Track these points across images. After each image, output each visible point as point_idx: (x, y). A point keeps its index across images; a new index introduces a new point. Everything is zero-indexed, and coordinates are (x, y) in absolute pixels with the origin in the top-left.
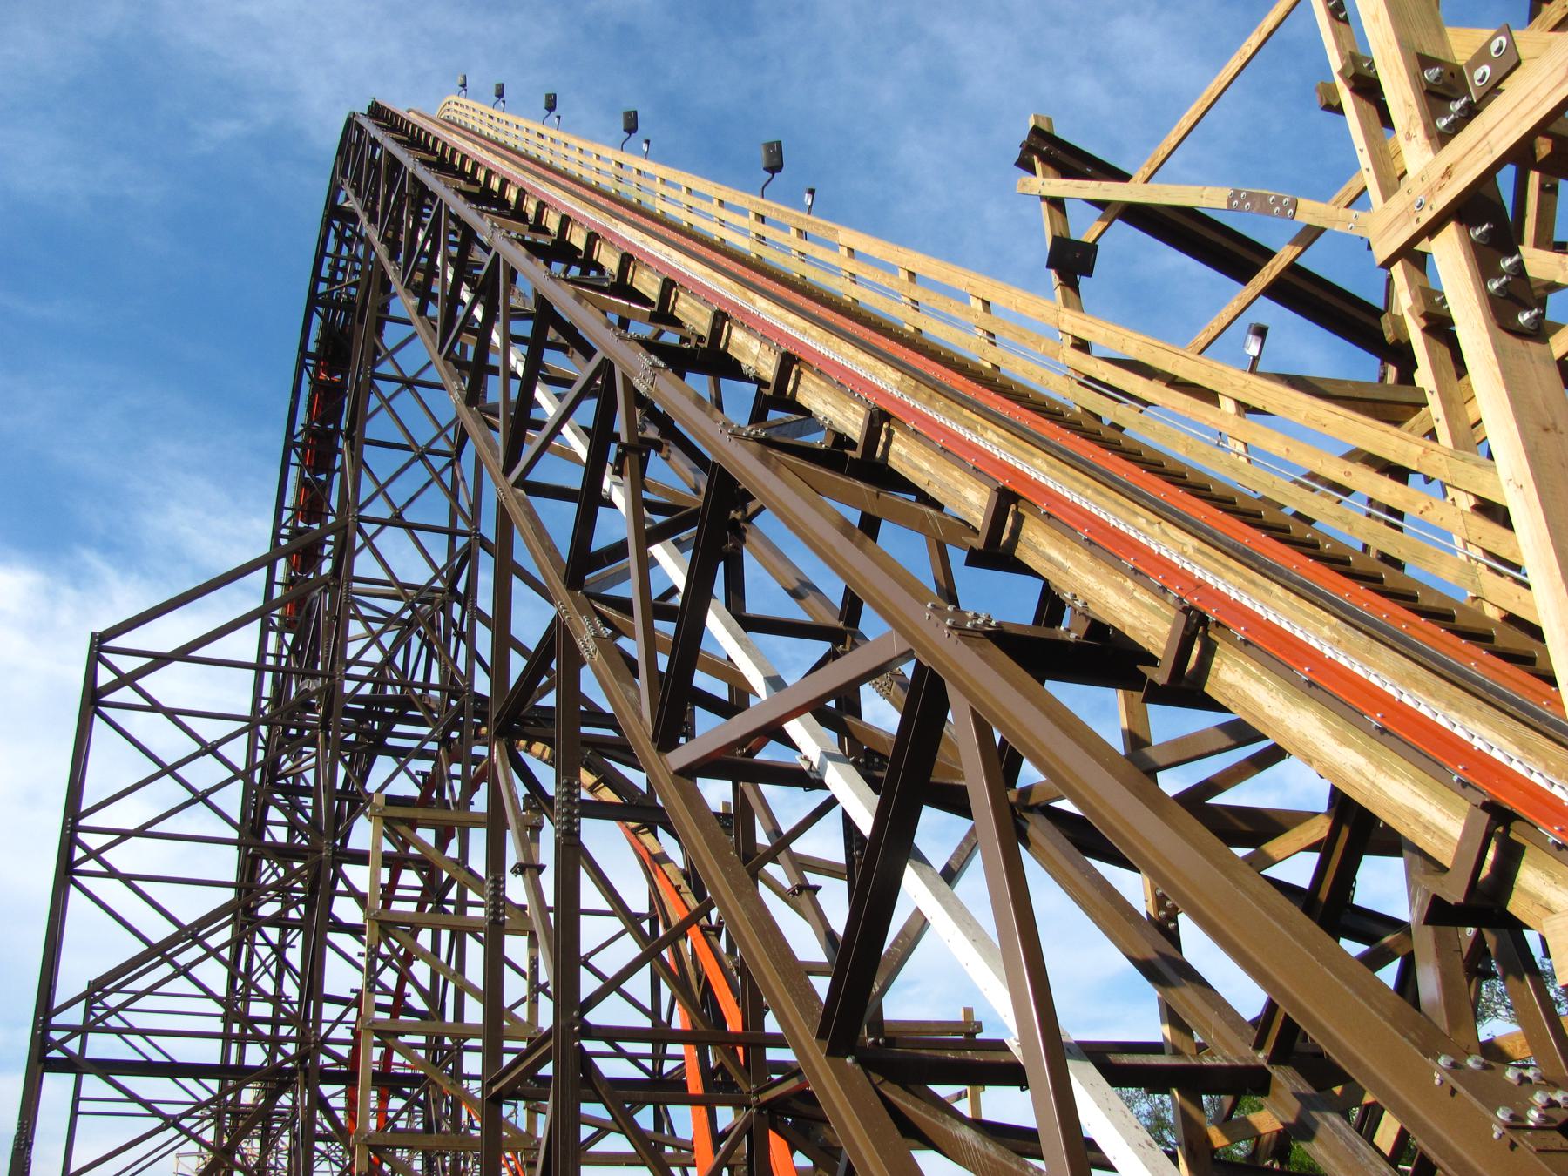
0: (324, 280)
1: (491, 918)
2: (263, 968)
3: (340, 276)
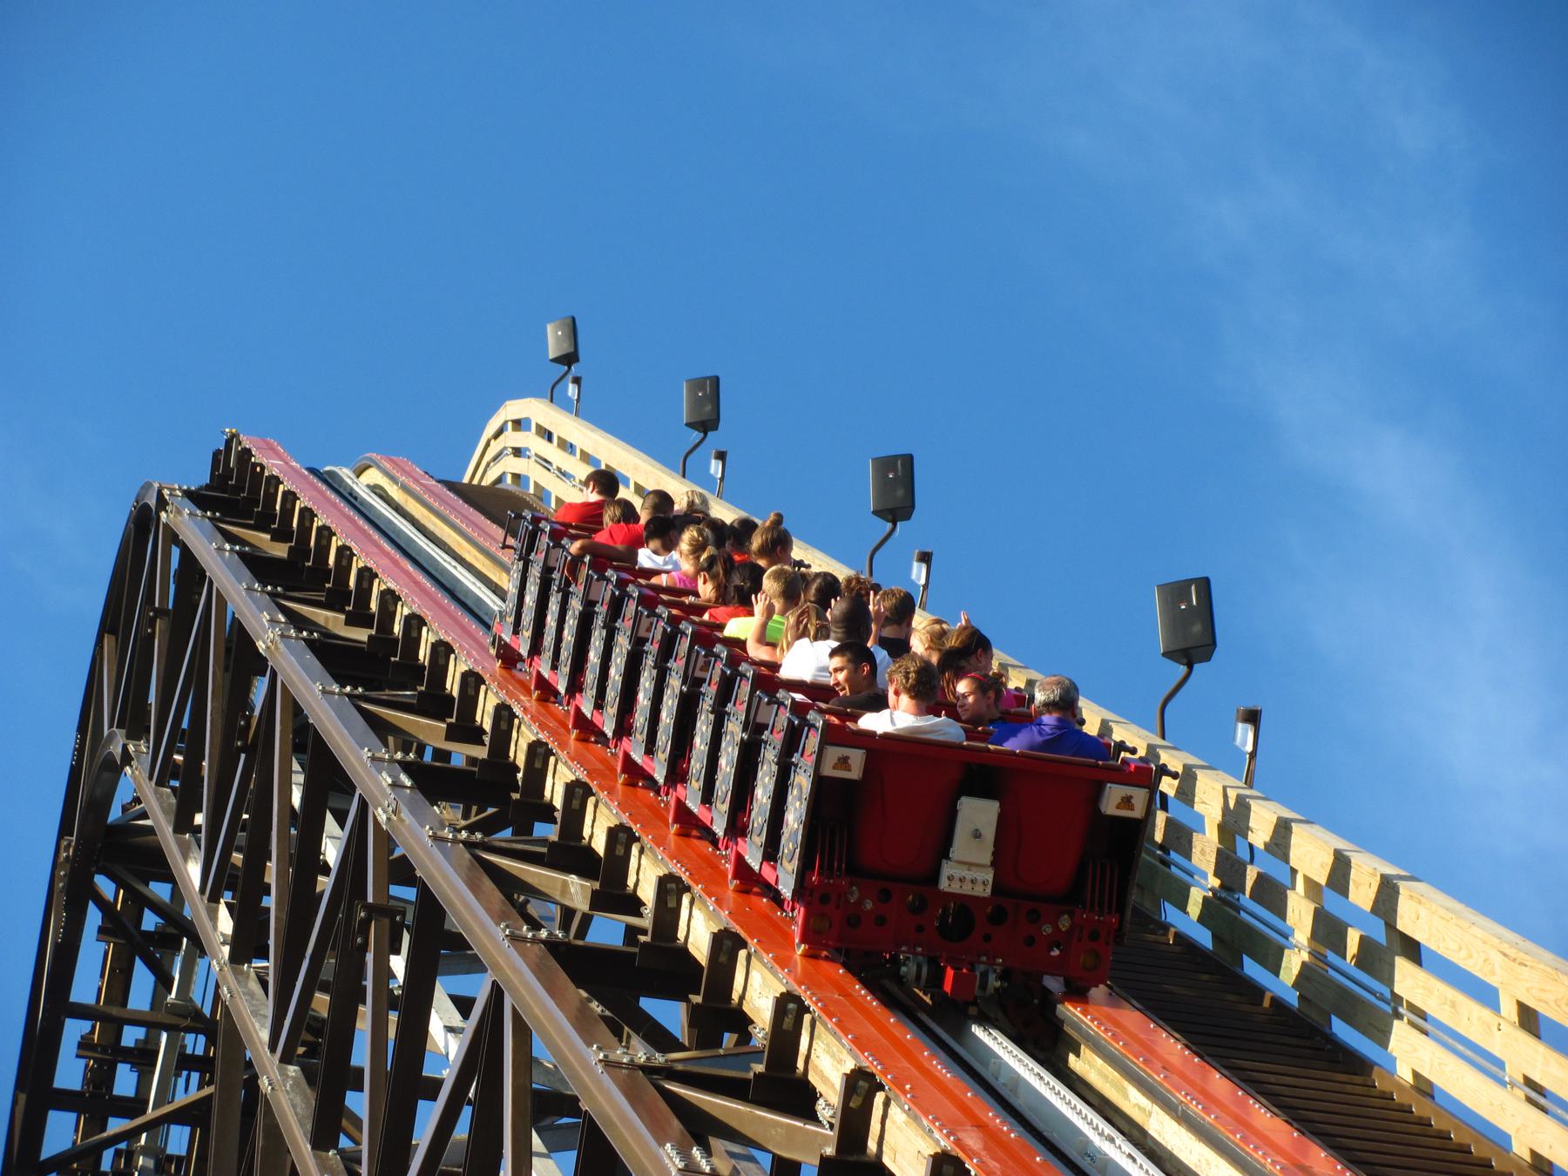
0: (66, 1100)
3: (125, 1081)
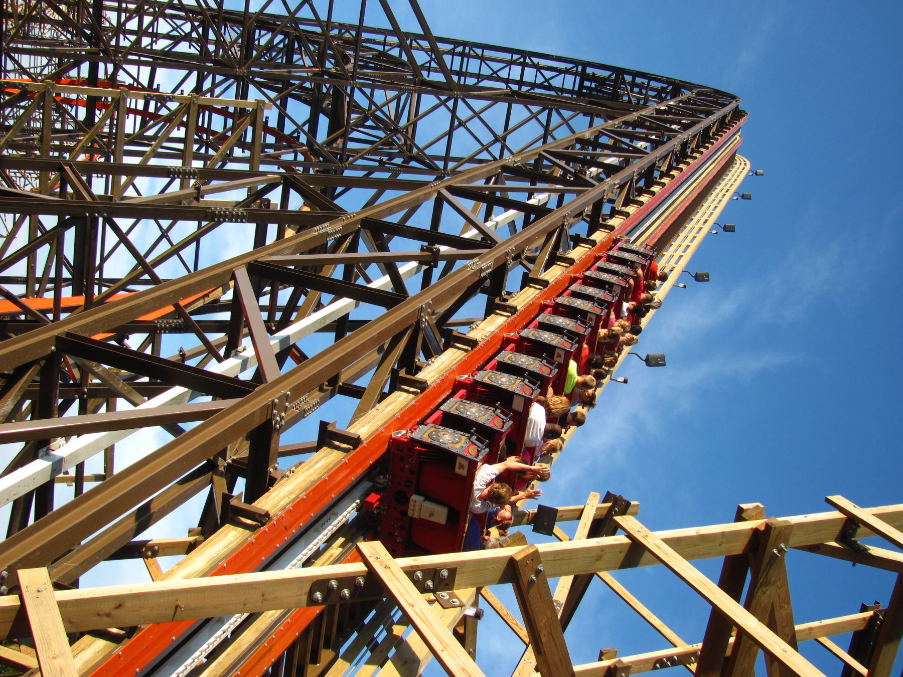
0: (634, 80)
1: (172, 170)
2: (175, 26)
3: (636, 90)
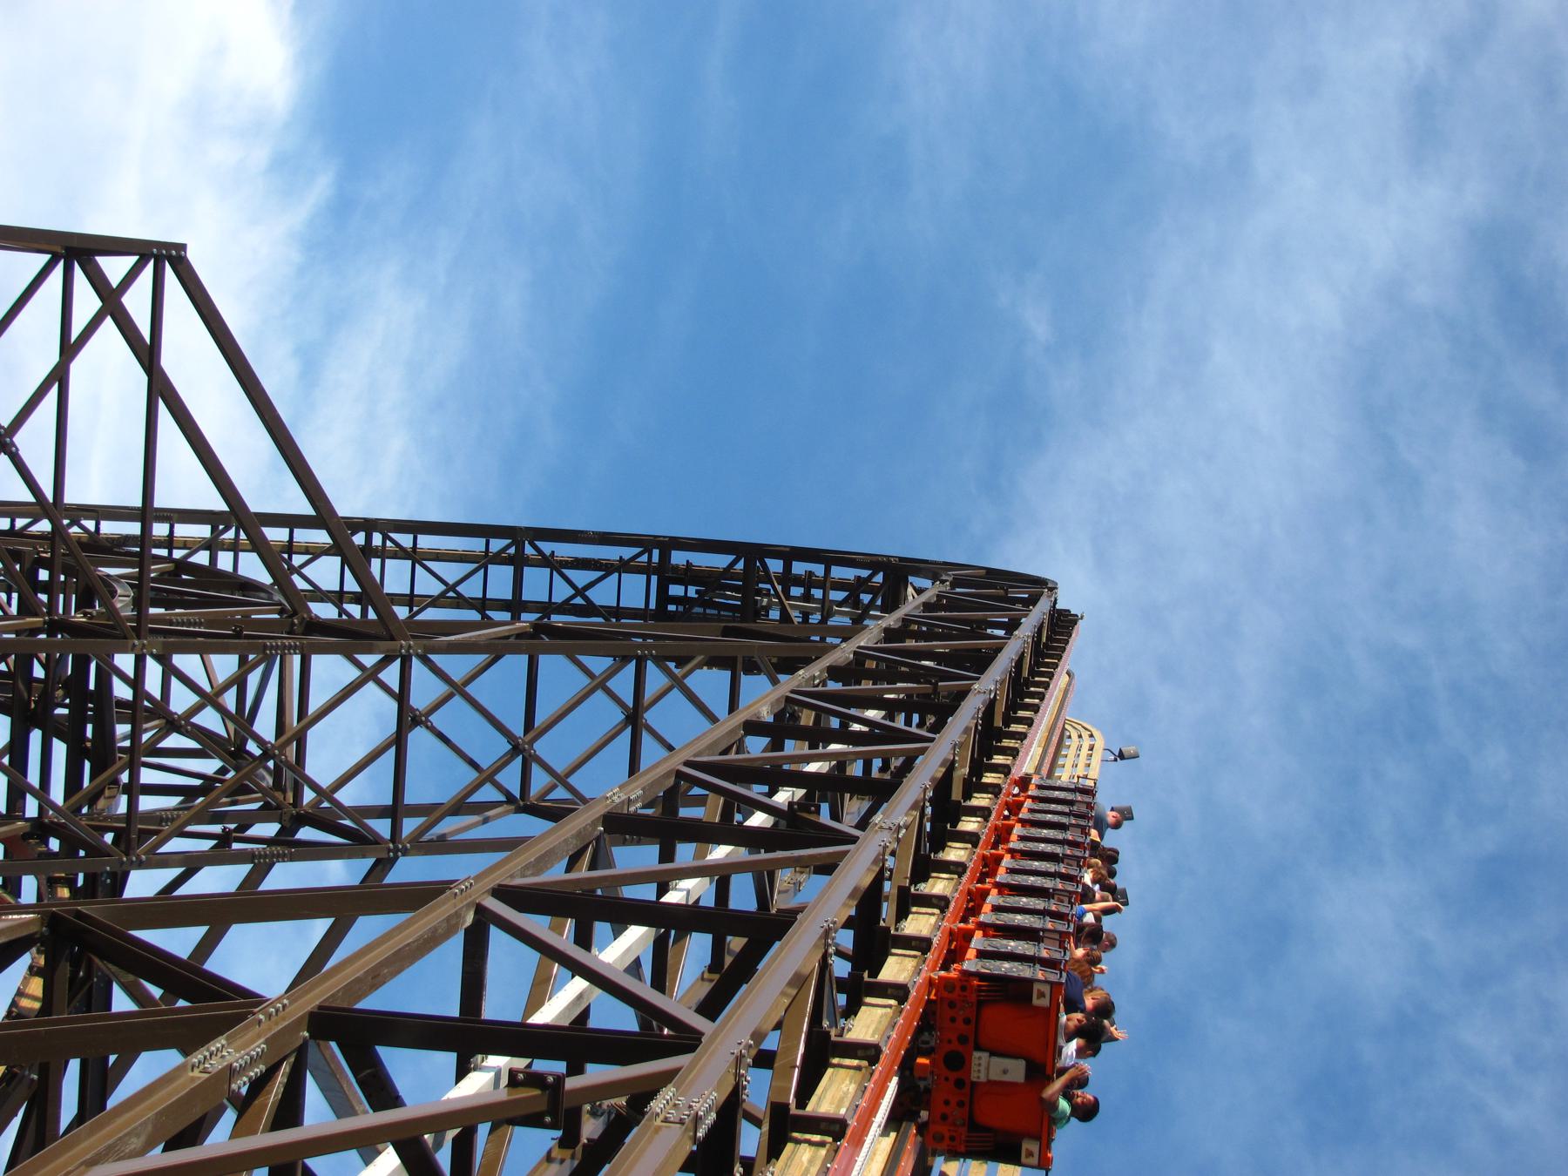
0: (787, 567)
3: (796, 591)
